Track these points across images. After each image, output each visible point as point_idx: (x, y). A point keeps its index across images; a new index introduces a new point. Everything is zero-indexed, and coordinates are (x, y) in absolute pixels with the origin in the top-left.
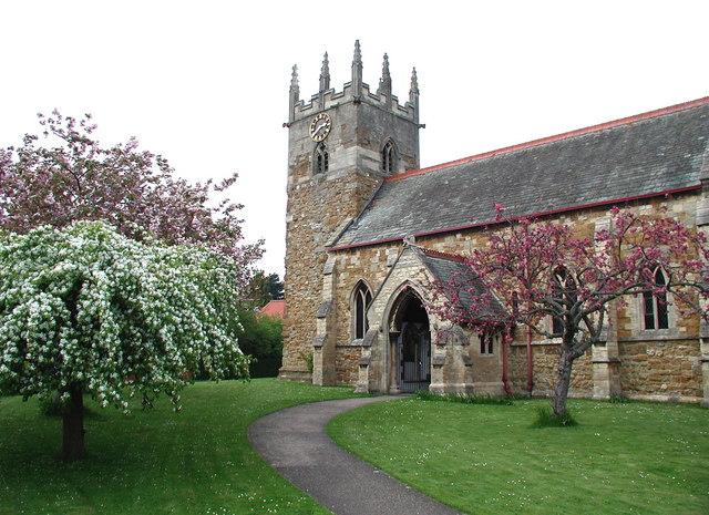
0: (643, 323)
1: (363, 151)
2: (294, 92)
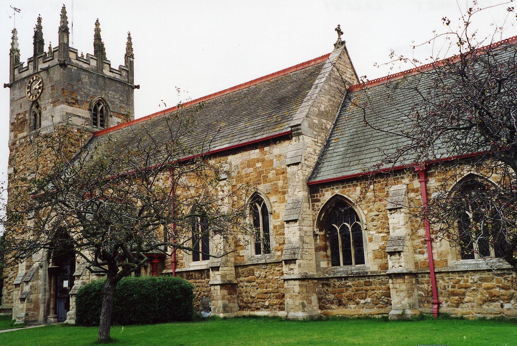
0: (254, 252)
1: (70, 109)
2: (14, 54)
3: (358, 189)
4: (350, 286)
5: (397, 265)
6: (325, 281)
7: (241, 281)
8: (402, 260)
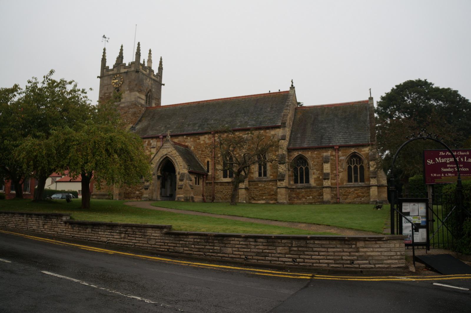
0: (258, 175)
2: (104, 60)
3: (310, 153)
4: (303, 192)
5: (327, 184)
6: (292, 190)
7: (251, 188)
8: (329, 182)
